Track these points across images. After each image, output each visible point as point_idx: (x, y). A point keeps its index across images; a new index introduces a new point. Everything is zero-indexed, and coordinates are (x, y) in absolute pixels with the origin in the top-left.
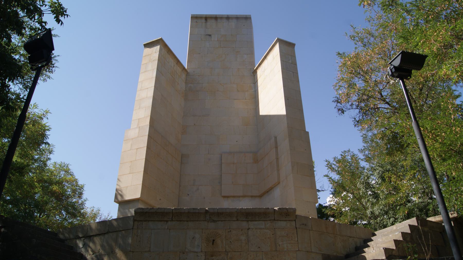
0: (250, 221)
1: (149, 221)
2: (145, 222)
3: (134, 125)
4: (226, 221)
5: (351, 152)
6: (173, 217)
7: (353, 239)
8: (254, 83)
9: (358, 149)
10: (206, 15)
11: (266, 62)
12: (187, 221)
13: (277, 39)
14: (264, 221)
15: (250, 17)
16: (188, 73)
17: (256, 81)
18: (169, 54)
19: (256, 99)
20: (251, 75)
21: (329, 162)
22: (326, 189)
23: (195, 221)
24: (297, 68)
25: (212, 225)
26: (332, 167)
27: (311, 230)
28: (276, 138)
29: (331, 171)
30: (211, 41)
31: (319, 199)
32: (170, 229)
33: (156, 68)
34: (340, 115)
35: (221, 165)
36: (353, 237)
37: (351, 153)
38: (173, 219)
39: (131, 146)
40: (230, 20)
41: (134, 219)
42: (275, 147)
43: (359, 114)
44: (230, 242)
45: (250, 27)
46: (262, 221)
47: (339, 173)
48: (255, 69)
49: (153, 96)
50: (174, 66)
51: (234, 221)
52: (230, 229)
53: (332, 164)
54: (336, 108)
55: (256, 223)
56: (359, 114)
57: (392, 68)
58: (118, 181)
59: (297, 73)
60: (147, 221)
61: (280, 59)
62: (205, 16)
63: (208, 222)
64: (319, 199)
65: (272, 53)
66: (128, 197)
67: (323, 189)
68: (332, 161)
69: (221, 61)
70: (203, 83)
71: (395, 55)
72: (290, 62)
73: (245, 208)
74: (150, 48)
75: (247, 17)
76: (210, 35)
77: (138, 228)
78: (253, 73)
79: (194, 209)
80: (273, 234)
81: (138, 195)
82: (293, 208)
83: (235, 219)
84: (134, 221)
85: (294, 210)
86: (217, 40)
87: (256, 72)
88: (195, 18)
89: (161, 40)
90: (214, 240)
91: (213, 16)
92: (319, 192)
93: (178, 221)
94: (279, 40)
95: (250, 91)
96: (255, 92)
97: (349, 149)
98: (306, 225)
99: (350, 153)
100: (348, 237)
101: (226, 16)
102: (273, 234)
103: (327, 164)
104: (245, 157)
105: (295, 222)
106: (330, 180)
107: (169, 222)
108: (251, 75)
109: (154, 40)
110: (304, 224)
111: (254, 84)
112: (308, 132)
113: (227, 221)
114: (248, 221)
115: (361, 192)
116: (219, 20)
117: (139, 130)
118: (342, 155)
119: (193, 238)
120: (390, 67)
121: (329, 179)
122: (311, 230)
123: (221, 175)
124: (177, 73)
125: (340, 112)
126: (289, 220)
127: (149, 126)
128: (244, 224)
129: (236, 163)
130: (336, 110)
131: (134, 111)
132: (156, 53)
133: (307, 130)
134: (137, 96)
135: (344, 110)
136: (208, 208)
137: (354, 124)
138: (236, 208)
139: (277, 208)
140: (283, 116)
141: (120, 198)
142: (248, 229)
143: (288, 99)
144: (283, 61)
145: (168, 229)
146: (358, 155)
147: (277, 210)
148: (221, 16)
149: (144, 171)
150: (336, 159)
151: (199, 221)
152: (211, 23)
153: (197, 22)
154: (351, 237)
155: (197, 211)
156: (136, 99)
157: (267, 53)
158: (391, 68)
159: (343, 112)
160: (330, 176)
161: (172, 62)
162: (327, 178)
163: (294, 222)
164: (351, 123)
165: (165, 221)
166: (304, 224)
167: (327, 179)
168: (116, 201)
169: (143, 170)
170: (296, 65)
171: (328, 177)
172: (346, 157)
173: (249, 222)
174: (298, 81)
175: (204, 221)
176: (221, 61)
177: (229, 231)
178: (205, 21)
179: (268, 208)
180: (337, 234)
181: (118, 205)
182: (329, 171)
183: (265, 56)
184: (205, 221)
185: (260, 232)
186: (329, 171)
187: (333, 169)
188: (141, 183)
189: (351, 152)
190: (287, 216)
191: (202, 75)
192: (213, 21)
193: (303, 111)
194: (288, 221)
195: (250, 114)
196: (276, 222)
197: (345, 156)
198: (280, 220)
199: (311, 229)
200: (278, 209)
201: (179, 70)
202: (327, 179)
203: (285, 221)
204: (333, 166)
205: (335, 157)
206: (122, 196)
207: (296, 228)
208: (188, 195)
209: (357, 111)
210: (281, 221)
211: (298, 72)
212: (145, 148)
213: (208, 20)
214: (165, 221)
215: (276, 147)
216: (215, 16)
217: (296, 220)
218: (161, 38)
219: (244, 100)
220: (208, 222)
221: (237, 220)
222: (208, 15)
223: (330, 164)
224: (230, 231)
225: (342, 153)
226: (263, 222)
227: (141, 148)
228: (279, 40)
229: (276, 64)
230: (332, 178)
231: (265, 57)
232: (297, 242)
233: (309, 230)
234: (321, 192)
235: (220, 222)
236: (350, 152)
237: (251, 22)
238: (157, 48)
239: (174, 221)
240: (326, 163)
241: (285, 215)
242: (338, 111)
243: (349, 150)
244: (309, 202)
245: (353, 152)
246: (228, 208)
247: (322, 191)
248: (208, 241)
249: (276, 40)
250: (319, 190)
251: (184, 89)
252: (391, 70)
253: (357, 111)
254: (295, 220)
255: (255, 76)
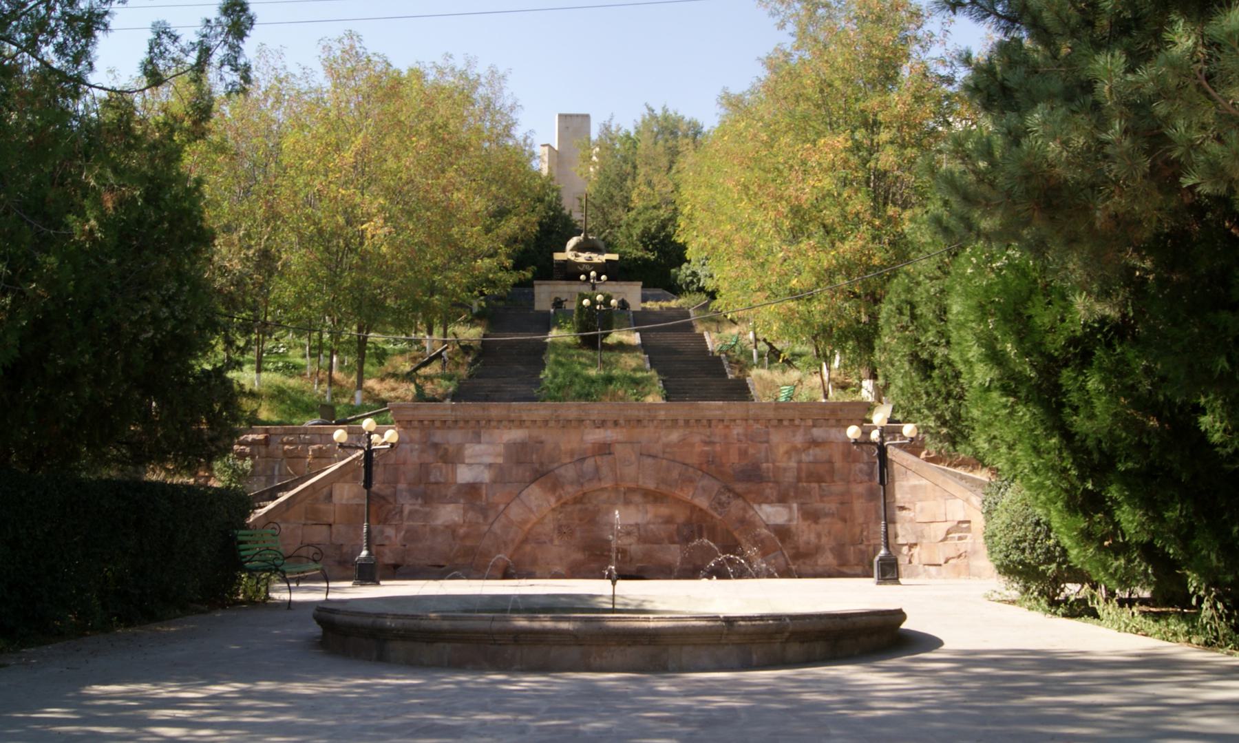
88: (560, 116)
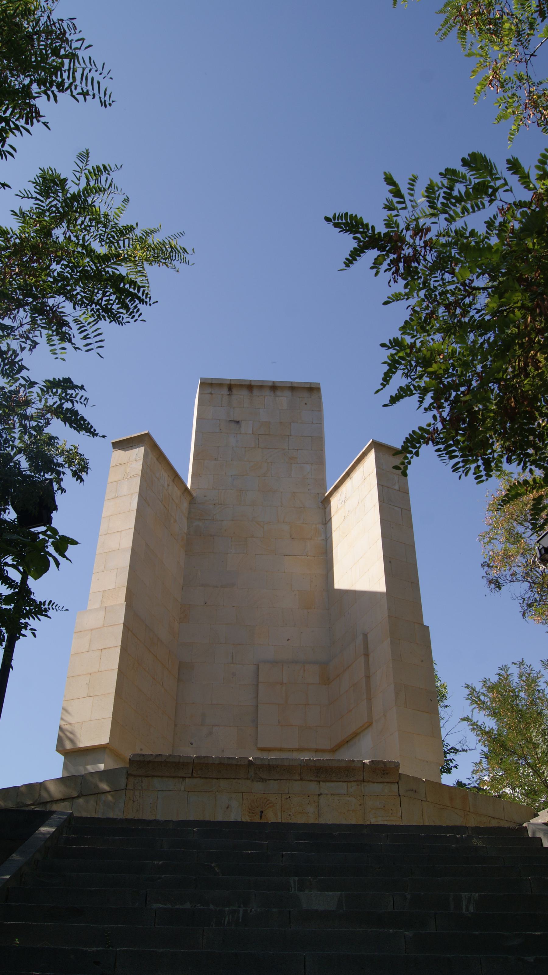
0: (323, 781)
1: (153, 776)
2: (146, 778)
3: (94, 603)
4: (282, 781)
5: (527, 666)
6: (194, 772)
7: (498, 822)
8: (324, 523)
9: (541, 661)
10: (230, 380)
11: (348, 484)
12: (218, 779)
13: (372, 442)
14: (345, 782)
15: (317, 386)
16: (193, 498)
17: (327, 520)
18: (160, 463)
19: (327, 557)
20: (319, 508)
21: (472, 688)
22: (471, 749)
23: (231, 779)
24: (409, 500)
25: (258, 786)
26: (480, 700)
27: (424, 801)
28: (365, 636)
29: (478, 709)
30: (241, 433)
31: (457, 768)
32: (188, 791)
33: (138, 491)
34: (493, 591)
35: (258, 685)
36: (499, 819)
37: (526, 667)
38: (194, 775)
39: (90, 643)
40: (279, 393)
41: (128, 772)
42: (364, 654)
43: (529, 591)
44: (290, 815)
45: (318, 407)
46: (343, 782)
47: (494, 714)
48: (326, 495)
49: (132, 547)
50: (168, 485)
51: (296, 780)
52: (288, 793)
53: (480, 694)
54: (485, 579)
55: (333, 784)
56: (529, 591)
57: (542, 549)
58: (64, 712)
59: (409, 510)
60: (150, 776)
61: (376, 483)
62: (228, 383)
63: (252, 781)
64: (457, 768)
65: (362, 467)
66: (84, 742)
67: (465, 747)
68: (478, 687)
69: (259, 477)
70: (222, 520)
71: (538, 537)
72: (397, 487)
73: (315, 759)
74: (125, 451)
75: (313, 388)
76: (238, 422)
77: (134, 788)
78: (321, 503)
79: (229, 758)
80: (360, 805)
81: (103, 738)
82: (394, 761)
83: (297, 777)
84: (129, 775)
85: (397, 766)
86: (251, 432)
87: (329, 502)
89: (148, 435)
90: (262, 812)
91: (243, 383)
92: (456, 754)
93: (203, 778)
94: (377, 446)
95: (316, 539)
96: (326, 541)
97: (522, 659)
98: (416, 791)
99: (526, 668)
100: (490, 818)
101: (271, 384)
102: (360, 805)
103: (469, 693)
104: (304, 671)
105: (398, 786)
106: (475, 727)
107: (187, 780)
108: (319, 508)
109: (133, 436)
110: (412, 790)
111: (323, 524)
112: (427, 627)
113: (283, 780)
114: (319, 781)
115: (540, 751)
116: (256, 392)
117: (105, 614)
118: (499, 674)
119: (228, 808)
120: (539, 546)
121: (471, 725)
122: (424, 801)
123: (257, 706)
124: (173, 499)
125: (493, 586)
126: (388, 783)
127: (125, 606)
128: (313, 787)
129: (286, 683)
130: (485, 582)
131: (93, 576)
132: (136, 460)
133: (425, 623)
134: (99, 544)
135: (500, 583)
136: (253, 758)
137: (520, 612)
138: (299, 759)
139: (369, 761)
140: (381, 594)
141: (68, 746)
142: (319, 795)
143: (390, 562)
144: (382, 486)
145: (185, 791)
146: (541, 674)
147: (368, 764)
148: (260, 384)
149: (116, 693)
150: (488, 684)
151: (238, 779)
152: (240, 395)
153: (211, 394)
154: (494, 818)
155: (234, 762)
156: (97, 552)
157: (352, 466)
158: (540, 548)
159: (499, 586)
160: (475, 720)
161: (164, 477)
162: (469, 723)
163: (396, 785)
164: (517, 608)
165: (181, 777)
166: (412, 790)
167: (469, 725)
168: (60, 749)
169: (113, 690)
170: (407, 493)
171: (471, 723)
172: (508, 678)
173: (321, 783)
174: (411, 527)
175: (245, 779)
176: (259, 477)
177: (288, 798)
178: (229, 393)
179: (353, 761)
180: (469, 812)
181: (62, 758)
182: (475, 708)
183: (347, 472)
184: (248, 779)
185: (339, 800)
186: (475, 708)
187: (481, 705)
188: (110, 715)
189: (527, 666)
190: (384, 774)
191: (221, 504)
192: (245, 392)
193: (418, 584)
194: (385, 784)
195: (316, 586)
196: (366, 784)
197: (508, 675)
198: (372, 782)
199: (425, 800)
200: (369, 762)
201: (177, 492)
202: (469, 725)
203: (381, 782)
204: (482, 698)
205: (485, 678)
206: (72, 741)
207: (400, 796)
208: (192, 744)
209: (527, 585)
210: (374, 782)
211: (410, 508)
212: (118, 650)
213: (234, 391)
214: (181, 777)
215: (367, 655)
216: (248, 383)
217: (399, 783)
218: (147, 432)
219: (303, 557)
220: (252, 781)
221: (301, 779)
222: (233, 380)
223: (475, 693)
224: (290, 797)
225: (501, 671)
226: (345, 784)
227: (109, 648)
228: (377, 446)
229: (370, 491)
230: (479, 723)
231: (348, 474)
232: (401, 819)
233: (422, 800)
234: (460, 753)
235: (272, 782)
236: (525, 666)
237: (320, 398)
238: (139, 452)
239: (196, 778)
240: (467, 691)
241: (381, 772)
242: (488, 583)
243: (523, 661)
244: (427, 762)
245: (531, 665)
246: (286, 759)
247: (463, 750)
248: (253, 813)
249: (370, 444)
250: (457, 748)
251: (186, 531)
252: (540, 551)
253: (527, 585)
254: (398, 783)
255: (327, 510)
